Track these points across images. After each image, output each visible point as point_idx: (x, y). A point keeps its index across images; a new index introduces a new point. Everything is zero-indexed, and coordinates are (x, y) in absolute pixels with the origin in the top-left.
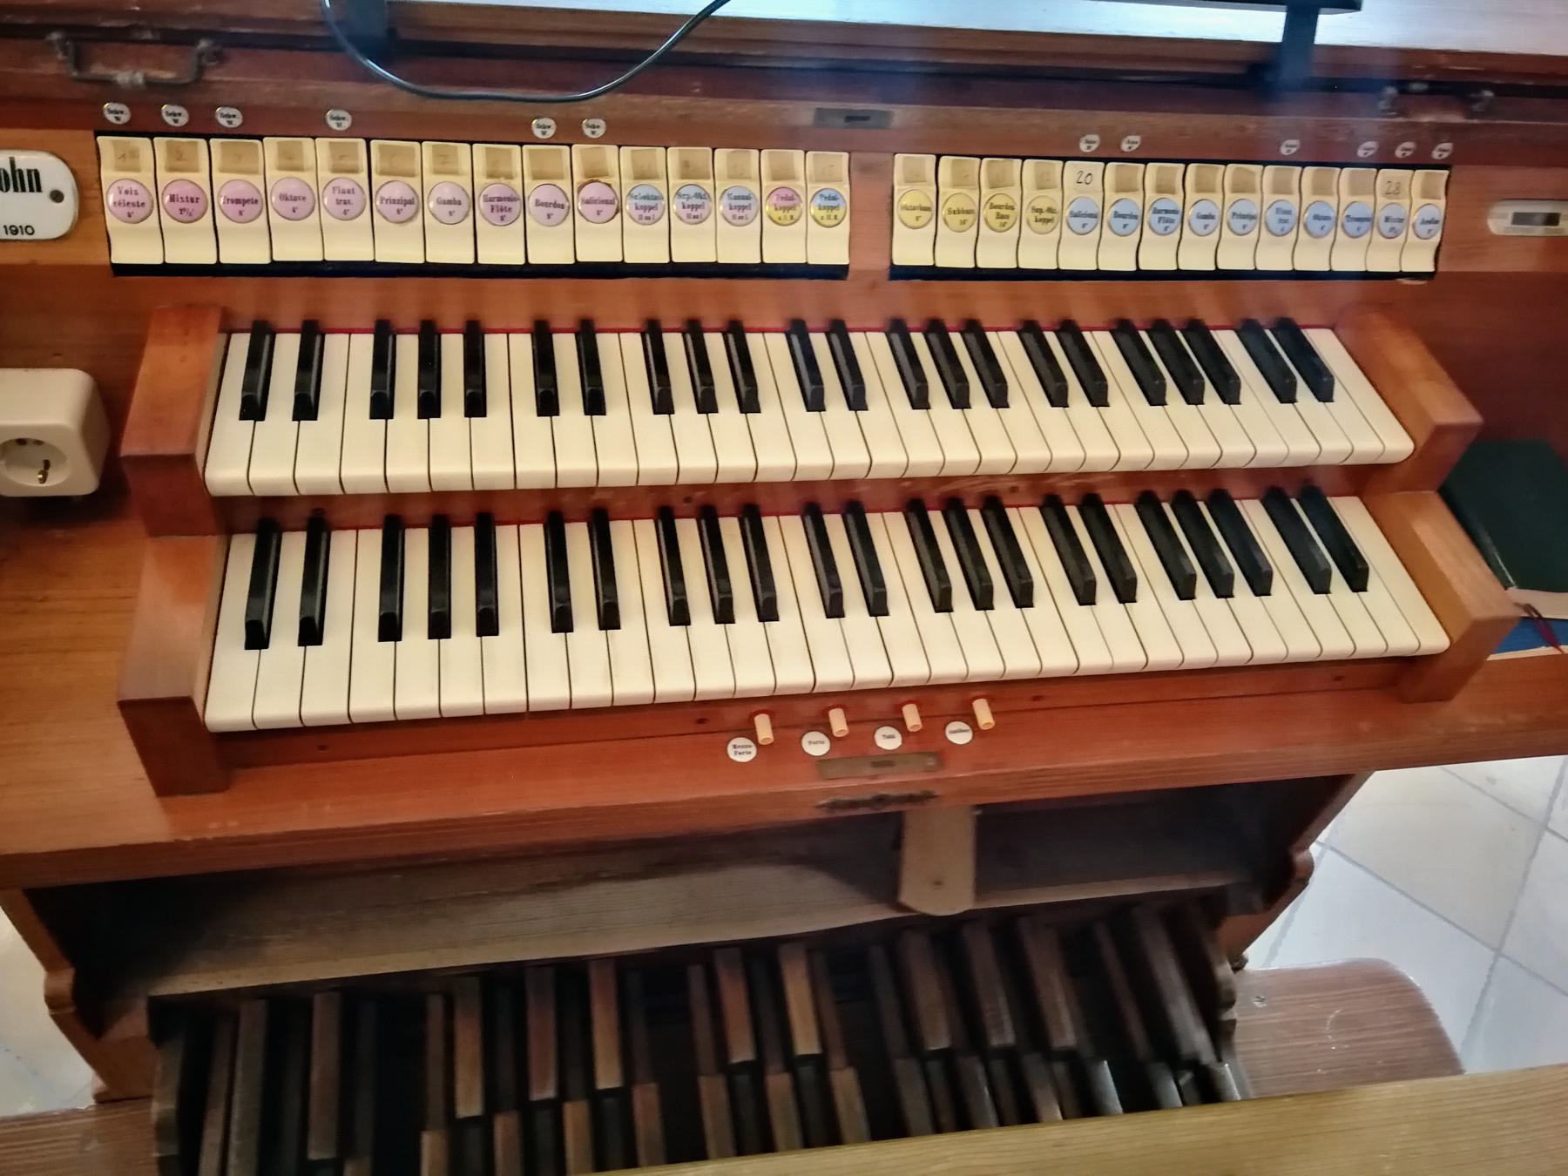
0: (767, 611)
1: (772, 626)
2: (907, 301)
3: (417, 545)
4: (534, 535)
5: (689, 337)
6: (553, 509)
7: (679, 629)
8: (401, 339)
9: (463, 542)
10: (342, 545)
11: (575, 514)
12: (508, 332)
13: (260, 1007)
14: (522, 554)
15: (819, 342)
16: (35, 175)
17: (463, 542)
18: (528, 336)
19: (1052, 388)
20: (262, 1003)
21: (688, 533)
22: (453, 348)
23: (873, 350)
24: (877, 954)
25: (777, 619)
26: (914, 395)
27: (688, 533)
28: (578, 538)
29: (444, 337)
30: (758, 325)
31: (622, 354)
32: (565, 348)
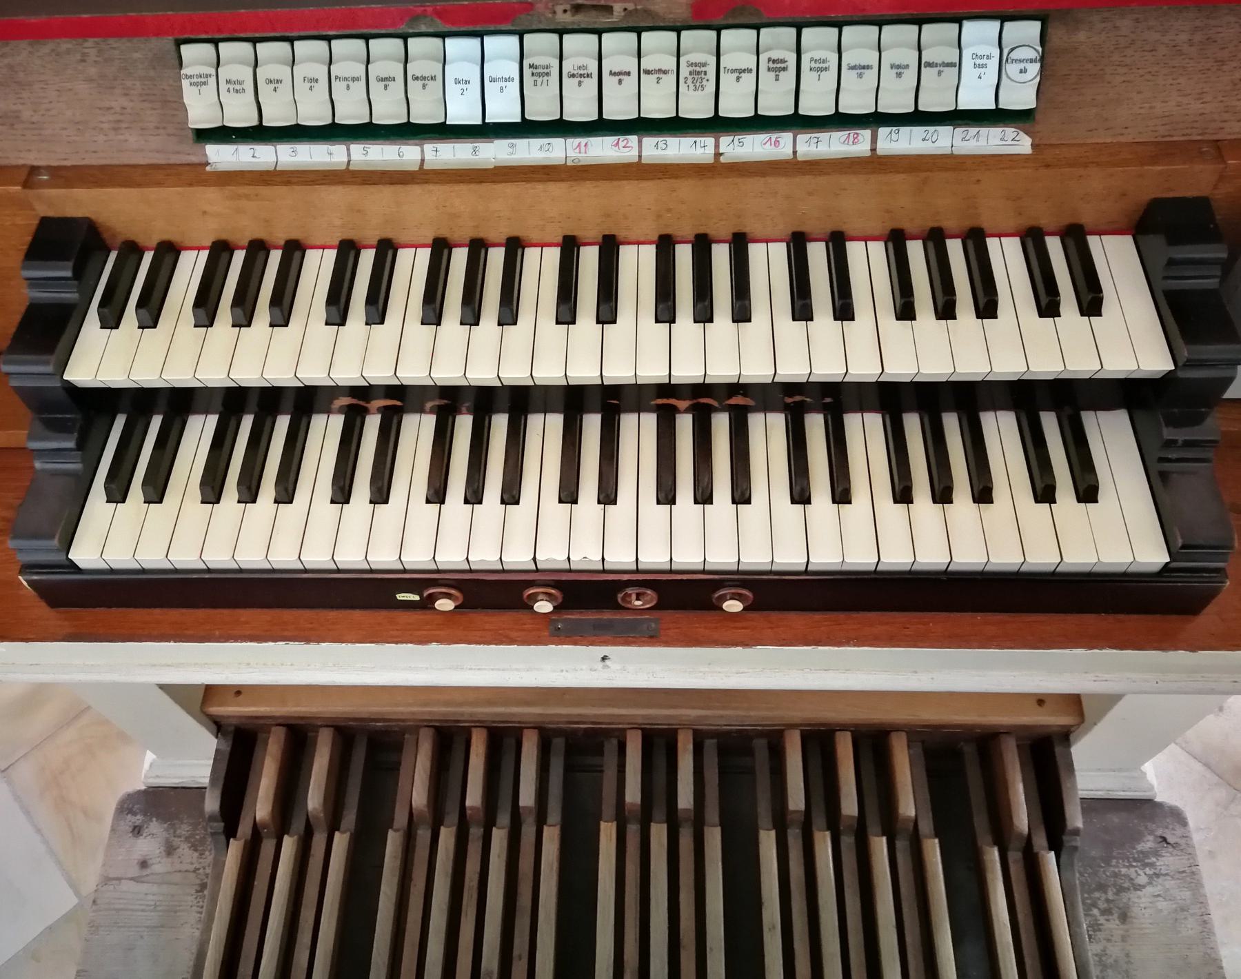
0: (983, 495)
1: (845, 508)
3: (464, 425)
4: (778, 421)
5: (890, 245)
6: (794, 399)
7: (799, 508)
9: (721, 424)
10: (535, 422)
11: (378, 407)
12: (767, 241)
13: (848, 736)
14: (768, 434)
15: (1054, 246)
16: (17, 116)
17: (721, 424)
18: (727, 245)
19: (1044, 300)
20: (640, 732)
21: (912, 424)
22: (721, 256)
23: (1007, 257)
26: (940, 308)
27: (912, 424)
28: (815, 425)
29: (622, 248)
31: (868, 263)
32: (817, 254)
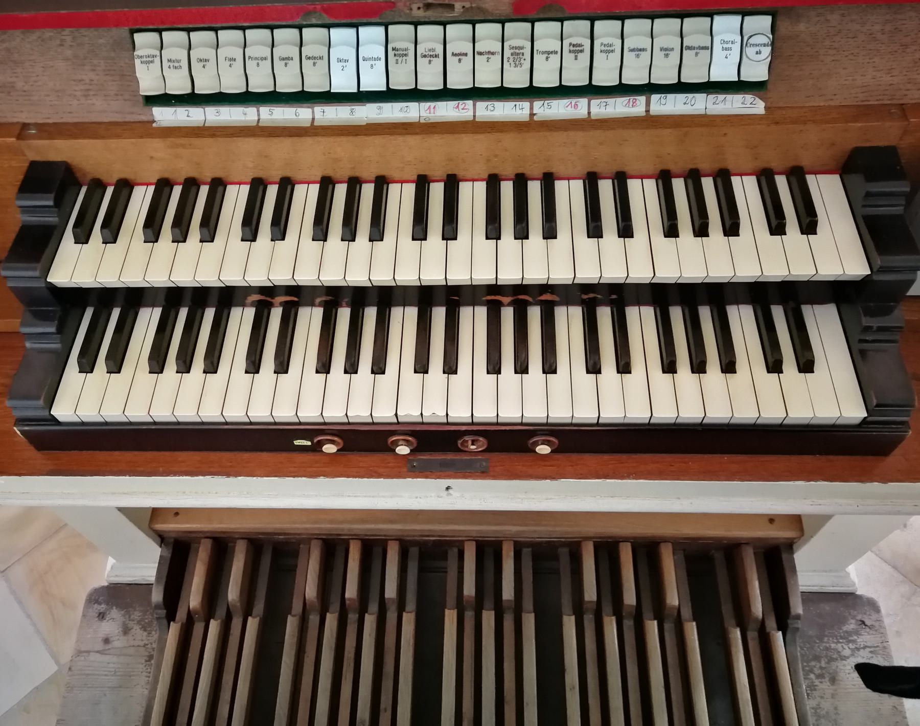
0: (729, 367)
1: (626, 377)
2: (675, 155)
3: (344, 315)
4: (576, 312)
5: (660, 182)
6: (589, 296)
7: (592, 376)
8: (503, 184)
9: (534, 314)
10: (397, 313)
11: (280, 302)
12: (569, 179)
14: (569, 322)
16: (12, 86)
17: (534, 314)
18: (539, 182)
19: (774, 223)
21: (676, 314)
22: (534, 190)
23: (747, 191)
24: (564, 552)
25: (630, 372)
26: (697, 228)
27: (676, 314)
28: (604, 315)
30: (469, 176)
31: (643, 195)
32: (606, 188)
